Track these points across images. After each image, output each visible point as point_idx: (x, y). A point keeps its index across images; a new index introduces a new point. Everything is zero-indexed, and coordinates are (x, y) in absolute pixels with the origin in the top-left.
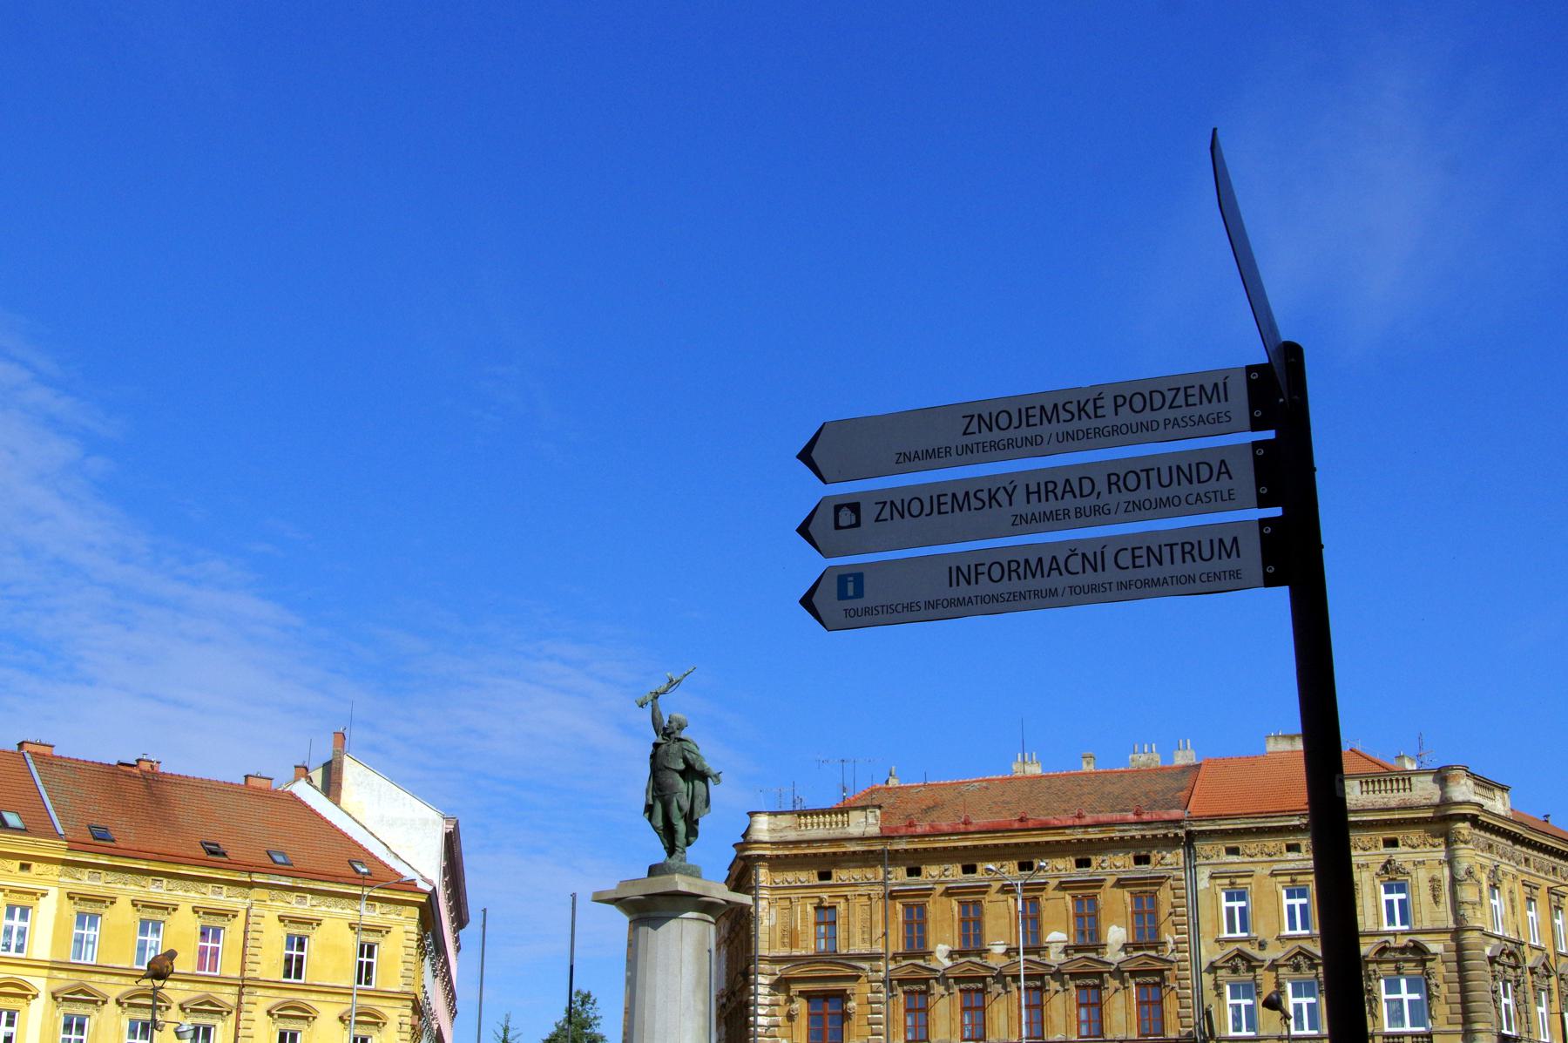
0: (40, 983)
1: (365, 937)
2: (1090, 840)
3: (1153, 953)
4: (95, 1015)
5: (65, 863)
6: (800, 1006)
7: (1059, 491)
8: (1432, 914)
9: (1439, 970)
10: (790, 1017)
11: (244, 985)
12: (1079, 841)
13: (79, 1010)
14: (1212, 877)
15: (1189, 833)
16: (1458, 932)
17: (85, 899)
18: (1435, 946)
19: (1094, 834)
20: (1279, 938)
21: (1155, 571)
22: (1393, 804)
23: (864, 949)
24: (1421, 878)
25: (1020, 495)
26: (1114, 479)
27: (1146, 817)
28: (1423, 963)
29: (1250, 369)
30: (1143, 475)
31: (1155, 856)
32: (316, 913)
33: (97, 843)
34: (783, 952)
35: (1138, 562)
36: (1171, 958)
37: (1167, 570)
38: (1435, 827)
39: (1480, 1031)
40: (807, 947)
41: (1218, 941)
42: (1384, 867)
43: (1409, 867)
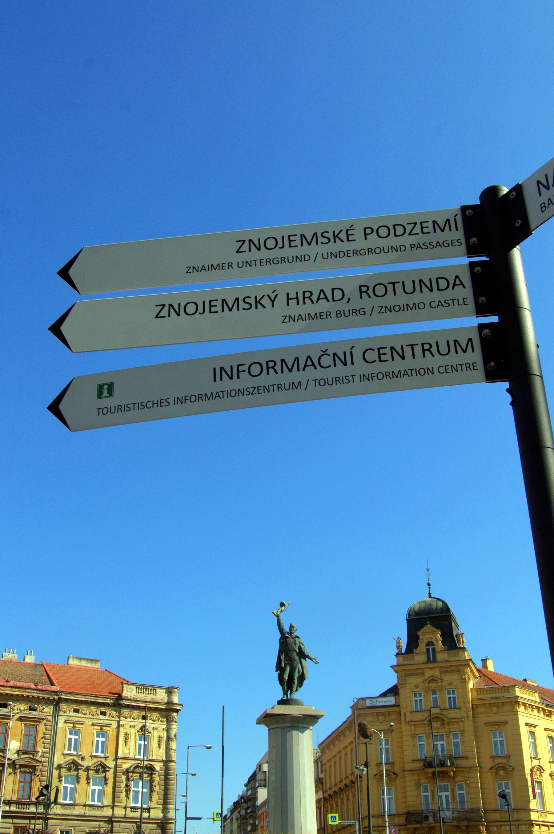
2: (12, 695)
3: (31, 756)
7: (314, 298)
8: (157, 753)
9: (156, 778)
12: (7, 694)
14: (65, 722)
15: (60, 698)
16: (167, 761)
18: (158, 767)
19: (15, 692)
20: (91, 756)
21: (398, 365)
22: (148, 700)
24: (155, 735)
25: (281, 300)
26: (364, 289)
27: (39, 687)
28: (151, 775)
29: (464, 209)
30: (390, 287)
31: (39, 707)
35: (383, 358)
36: (40, 759)
37: (409, 363)
38: (163, 713)
39: (171, 809)
41: (63, 754)
42: (141, 729)
43: (151, 730)
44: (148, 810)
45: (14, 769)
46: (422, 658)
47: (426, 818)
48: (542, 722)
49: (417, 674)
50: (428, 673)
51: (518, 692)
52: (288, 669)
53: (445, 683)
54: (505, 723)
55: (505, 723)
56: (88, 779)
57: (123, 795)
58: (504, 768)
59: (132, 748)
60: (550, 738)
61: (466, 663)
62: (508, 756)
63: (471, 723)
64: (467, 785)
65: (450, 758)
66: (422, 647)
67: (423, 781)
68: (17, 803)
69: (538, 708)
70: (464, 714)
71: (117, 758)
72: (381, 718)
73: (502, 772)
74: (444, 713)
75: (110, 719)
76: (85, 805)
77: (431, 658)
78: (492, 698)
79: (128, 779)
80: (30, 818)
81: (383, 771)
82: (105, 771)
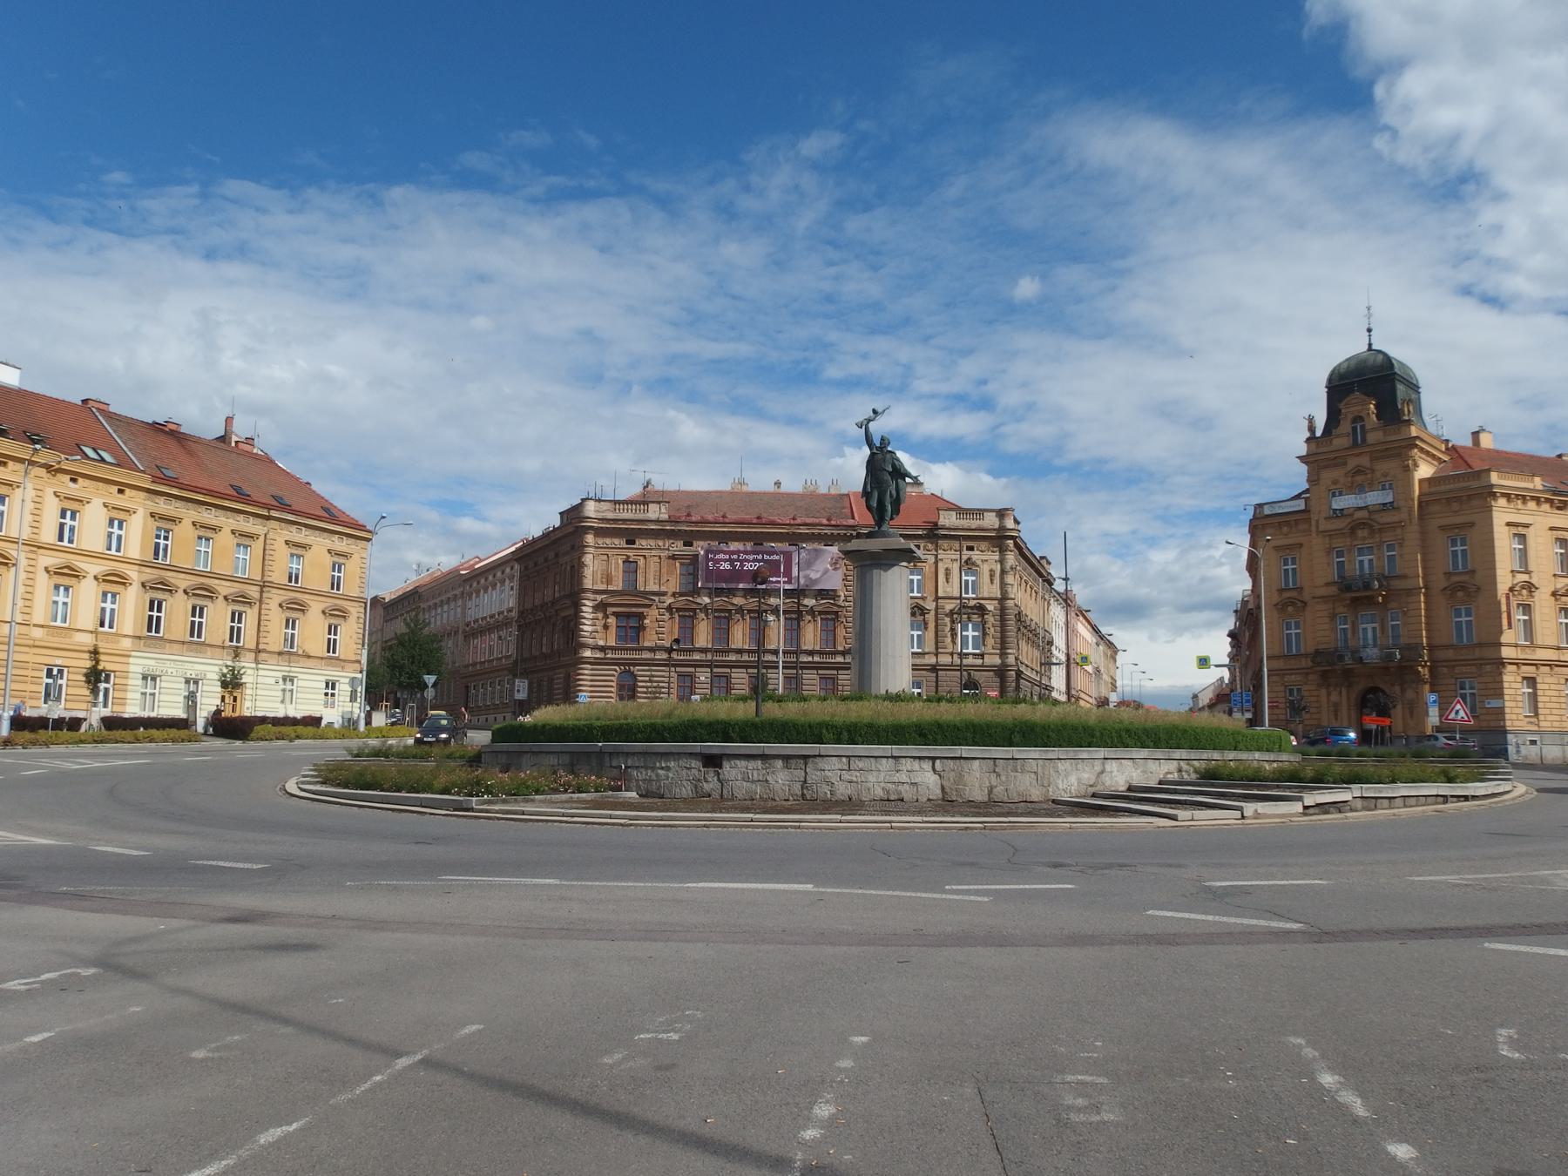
0: (133, 574)
1: (336, 559)
4: (171, 600)
5: (149, 491)
6: (612, 620)
8: (991, 590)
9: (990, 619)
10: (606, 627)
11: (264, 586)
13: (159, 595)
17: (163, 518)
19: (803, 530)
23: (655, 588)
24: (985, 569)
32: (307, 541)
33: (165, 483)
34: (603, 587)
40: (618, 585)
44: (982, 656)
47: (1341, 658)
48: (1543, 522)
49: (1335, 465)
50: (1353, 463)
51: (1494, 478)
52: (876, 494)
53: (1378, 474)
54: (1472, 525)
55: (1472, 525)
57: (949, 640)
58: (1463, 588)
59: (956, 585)
60: (1562, 542)
61: (1411, 443)
62: (1473, 572)
64: (1405, 613)
65: (1383, 578)
66: (1345, 426)
67: (1340, 609)
68: (820, 653)
69: (1537, 500)
71: (937, 598)
72: (1285, 529)
73: (1460, 594)
74: (1375, 516)
76: (1516, 646)
78: (1450, 491)
79: (953, 622)
80: (838, 669)
82: (923, 614)
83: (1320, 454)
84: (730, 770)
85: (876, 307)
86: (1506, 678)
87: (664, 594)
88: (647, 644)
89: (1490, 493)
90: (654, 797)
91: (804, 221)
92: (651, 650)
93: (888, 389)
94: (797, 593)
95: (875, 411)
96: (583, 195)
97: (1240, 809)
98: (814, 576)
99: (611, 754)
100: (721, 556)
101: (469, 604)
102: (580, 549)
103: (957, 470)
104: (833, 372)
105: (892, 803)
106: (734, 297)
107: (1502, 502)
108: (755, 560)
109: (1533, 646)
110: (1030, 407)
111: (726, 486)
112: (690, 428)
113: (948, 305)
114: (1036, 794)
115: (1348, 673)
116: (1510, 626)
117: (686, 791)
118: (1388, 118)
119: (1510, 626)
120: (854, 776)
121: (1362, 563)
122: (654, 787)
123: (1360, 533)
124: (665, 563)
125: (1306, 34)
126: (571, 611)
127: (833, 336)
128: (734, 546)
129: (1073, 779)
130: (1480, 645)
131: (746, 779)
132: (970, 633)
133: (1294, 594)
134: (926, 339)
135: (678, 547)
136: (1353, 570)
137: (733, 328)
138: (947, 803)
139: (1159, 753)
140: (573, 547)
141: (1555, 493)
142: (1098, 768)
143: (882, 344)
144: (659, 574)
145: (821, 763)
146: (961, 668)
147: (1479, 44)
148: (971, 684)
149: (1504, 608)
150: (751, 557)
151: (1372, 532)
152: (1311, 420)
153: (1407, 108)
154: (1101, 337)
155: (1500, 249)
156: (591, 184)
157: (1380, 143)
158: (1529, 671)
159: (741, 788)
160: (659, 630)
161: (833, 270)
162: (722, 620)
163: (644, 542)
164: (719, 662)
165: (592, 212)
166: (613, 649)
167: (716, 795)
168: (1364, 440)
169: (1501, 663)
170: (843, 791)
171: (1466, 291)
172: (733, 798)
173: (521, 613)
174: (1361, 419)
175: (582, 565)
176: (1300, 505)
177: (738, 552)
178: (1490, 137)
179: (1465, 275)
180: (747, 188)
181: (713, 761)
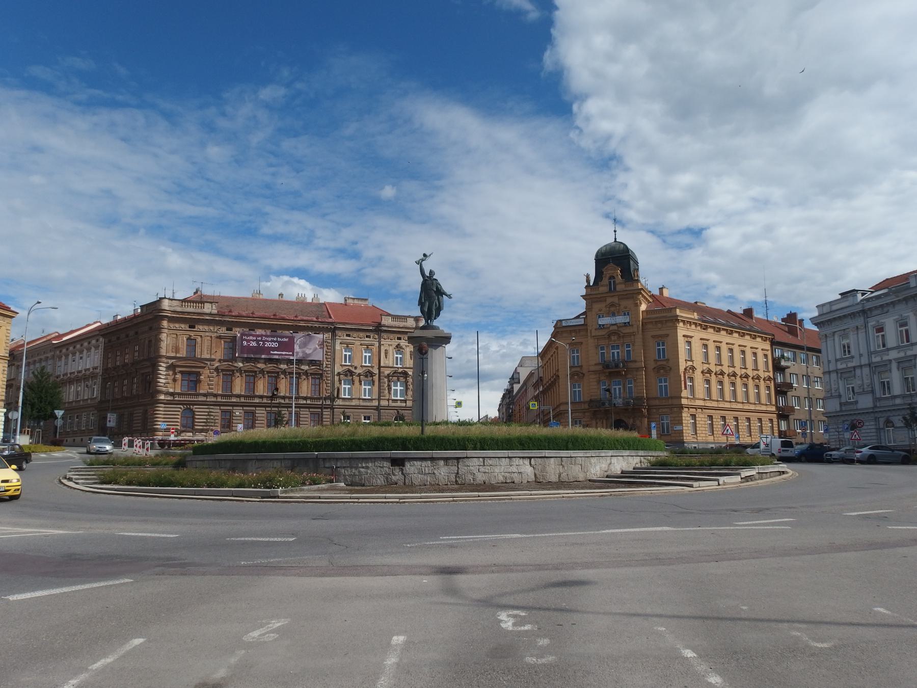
6: (179, 376)
10: (175, 380)
23: (208, 356)
28: (406, 378)
34: (173, 355)
40: (183, 353)
45: (307, 376)
46: (605, 289)
47: (604, 404)
48: (697, 334)
50: (609, 300)
51: (678, 312)
54: (667, 335)
55: (667, 335)
56: (360, 382)
58: (663, 368)
59: (391, 360)
61: (639, 292)
62: (668, 360)
63: (641, 336)
64: (635, 381)
65: (624, 362)
66: (605, 281)
67: (602, 378)
68: (311, 398)
69: (696, 324)
70: (635, 330)
71: (380, 367)
75: (373, 340)
76: (359, 399)
77: (612, 290)
79: (389, 381)
80: (255, 406)
81: (28, 364)
82: (372, 376)
83: (592, 294)
84: (409, 467)
85: (296, 194)
86: (684, 415)
87: (214, 360)
88: (201, 392)
89: (676, 320)
90: (356, 485)
91: (256, 139)
92: (205, 395)
93: (299, 243)
94: (300, 362)
95: (425, 255)
96: (114, 105)
97: (718, 480)
98: (308, 352)
99: (324, 459)
100: (251, 338)
101: (58, 364)
102: (159, 330)
103: (337, 293)
104: (266, 230)
105: (509, 485)
106: (208, 180)
107: (681, 324)
108: (272, 341)
109: (694, 398)
110: (380, 259)
111: (248, 295)
112: (175, 259)
113: (338, 197)
114: (581, 477)
115: (607, 412)
116: (686, 388)
117: (380, 481)
118: (579, 122)
119: (686, 388)
120: (487, 469)
121: (615, 354)
122: (357, 479)
123: (613, 338)
124: (214, 340)
125: (542, 74)
126: (150, 370)
127: (268, 209)
128: (259, 332)
129: (598, 468)
130: (672, 398)
131: (420, 472)
132: (399, 388)
133: (578, 369)
134: (324, 216)
135: (223, 331)
136: (608, 357)
137: (206, 198)
138: (539, 483)
139: (633, 453)
140: (151, 329)
141: (704, 321)
142: (609, 462)
143: (297, 216)
144: (210, 348)
145: (468, 462)
146: (393, 408)
147: (623, 93)
148: (400, 417)
149: (683, 379)
150: (270, 339)
151: (619, 337)
152: (588, 277)
153: (588, 119)
154: (424, 223)
155: (625, 196)
156: (120, 98)
157: (573, 135)
158: (693, 411)
159: (417, 479)
160: (210, 383)
161: (272, 170)
162: (252, 376)
163: (201, 327)
164: (249, 404)
165: (118, 116)
166: (179, 394)
167: (401, 483)
168: (615, 288)
169: (681, 407)
170: (480, 478)
171: (607, 216)
172: (412, 485)
173: (106, 370)
174: (614, 277)
175: (159, 340)
176: (581, 321)
177: (261, 336)
178: (624, 140)
179: (607, 208)
180: (223, 114)
181: (398, 463)
